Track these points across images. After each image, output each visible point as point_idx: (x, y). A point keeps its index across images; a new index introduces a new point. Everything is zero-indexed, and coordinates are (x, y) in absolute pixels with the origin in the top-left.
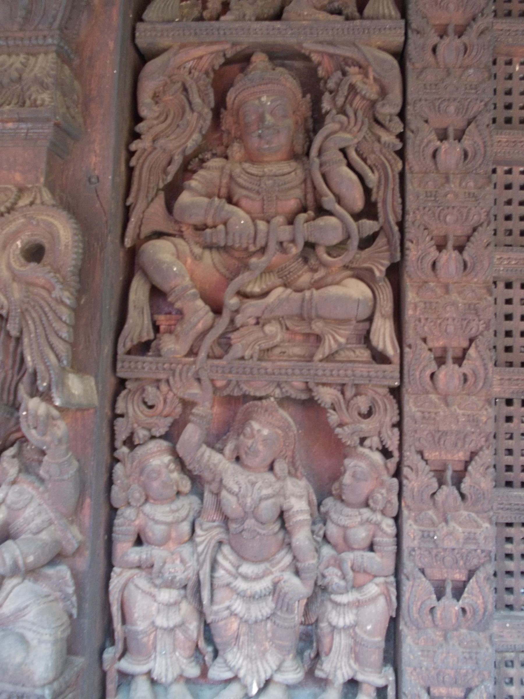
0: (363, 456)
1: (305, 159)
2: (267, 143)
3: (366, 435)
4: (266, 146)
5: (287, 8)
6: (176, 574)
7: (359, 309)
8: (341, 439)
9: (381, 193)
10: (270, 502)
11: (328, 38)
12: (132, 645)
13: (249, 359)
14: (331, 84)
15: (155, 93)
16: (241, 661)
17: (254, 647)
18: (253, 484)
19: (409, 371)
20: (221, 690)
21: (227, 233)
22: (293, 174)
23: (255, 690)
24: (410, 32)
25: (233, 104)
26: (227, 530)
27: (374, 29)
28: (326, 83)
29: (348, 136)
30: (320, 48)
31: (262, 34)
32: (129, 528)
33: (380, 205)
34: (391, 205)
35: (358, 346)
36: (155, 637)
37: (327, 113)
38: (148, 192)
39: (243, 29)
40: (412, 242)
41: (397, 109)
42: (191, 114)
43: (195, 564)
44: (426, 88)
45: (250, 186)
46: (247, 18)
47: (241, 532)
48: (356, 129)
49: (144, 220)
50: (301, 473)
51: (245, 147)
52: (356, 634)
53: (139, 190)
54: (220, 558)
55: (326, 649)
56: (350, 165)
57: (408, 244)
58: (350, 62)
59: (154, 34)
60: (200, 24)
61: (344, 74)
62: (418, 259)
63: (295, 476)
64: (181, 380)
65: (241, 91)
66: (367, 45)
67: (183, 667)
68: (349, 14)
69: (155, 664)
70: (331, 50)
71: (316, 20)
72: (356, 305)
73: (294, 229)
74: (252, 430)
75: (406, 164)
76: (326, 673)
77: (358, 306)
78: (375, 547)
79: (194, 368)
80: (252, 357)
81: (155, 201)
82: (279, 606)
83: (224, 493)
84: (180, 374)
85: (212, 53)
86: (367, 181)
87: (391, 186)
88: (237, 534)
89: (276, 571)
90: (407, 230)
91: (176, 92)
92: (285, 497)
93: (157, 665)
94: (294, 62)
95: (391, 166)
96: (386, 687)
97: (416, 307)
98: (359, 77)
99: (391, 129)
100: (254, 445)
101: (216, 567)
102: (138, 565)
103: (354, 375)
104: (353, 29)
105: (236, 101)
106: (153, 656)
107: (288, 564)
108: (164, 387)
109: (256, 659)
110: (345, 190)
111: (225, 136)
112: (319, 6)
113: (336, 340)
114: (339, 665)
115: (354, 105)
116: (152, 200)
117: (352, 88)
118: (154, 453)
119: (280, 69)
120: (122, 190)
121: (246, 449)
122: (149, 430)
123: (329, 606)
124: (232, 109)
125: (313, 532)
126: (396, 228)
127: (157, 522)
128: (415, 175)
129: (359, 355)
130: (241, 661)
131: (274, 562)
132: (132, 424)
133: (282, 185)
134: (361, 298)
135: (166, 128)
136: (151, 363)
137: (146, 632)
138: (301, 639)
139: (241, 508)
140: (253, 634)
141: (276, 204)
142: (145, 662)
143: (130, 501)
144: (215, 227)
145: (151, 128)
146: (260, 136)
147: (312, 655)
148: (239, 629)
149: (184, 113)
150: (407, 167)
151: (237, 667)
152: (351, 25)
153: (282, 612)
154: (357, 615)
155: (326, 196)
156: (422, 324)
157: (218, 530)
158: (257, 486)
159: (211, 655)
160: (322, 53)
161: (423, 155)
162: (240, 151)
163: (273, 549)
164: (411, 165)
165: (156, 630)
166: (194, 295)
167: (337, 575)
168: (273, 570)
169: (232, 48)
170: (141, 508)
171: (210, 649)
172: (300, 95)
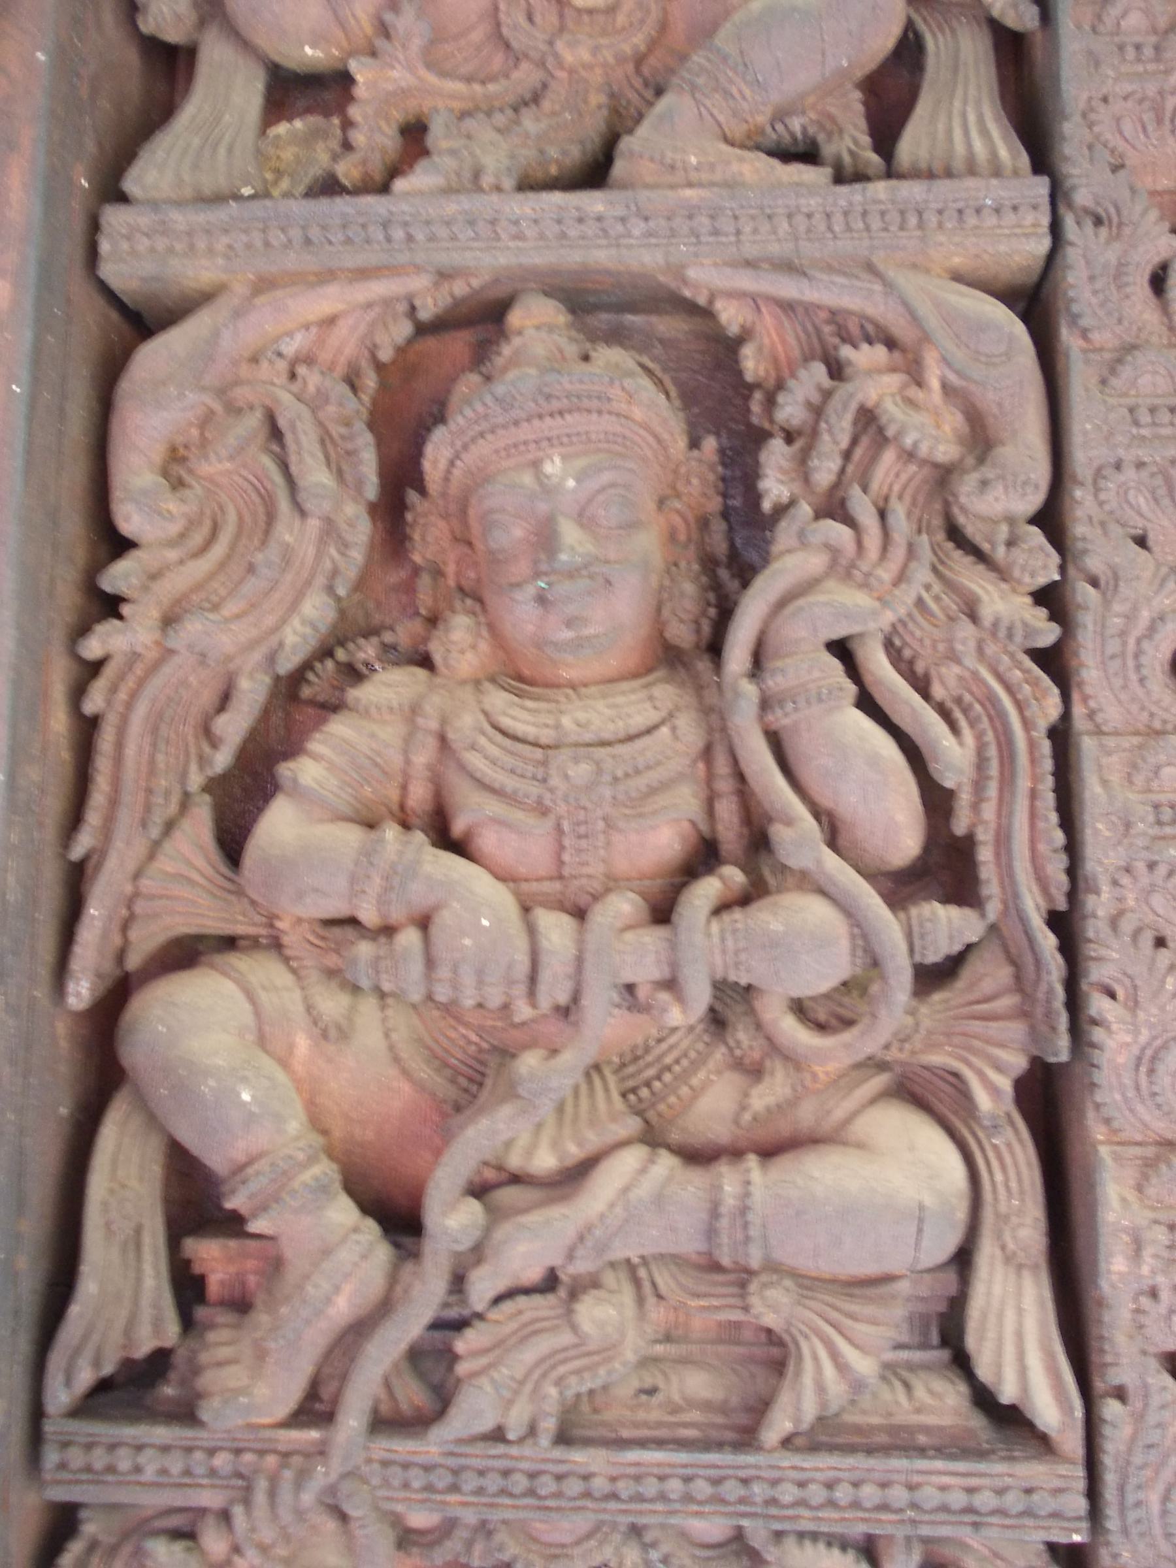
1: (703, 665)
2: (569, 624)
4: (567, 634)
5: (626, 144)
7: (925, 1243)
9: (989, 811)
11: (774, 249)
13: (521, 1441)
14: (791, 410)
15: (173, 449)
19: (1121, 1489)
21: (430, 963)
22: (665, 730)
24: (1069, 221)
25: (447, 479)
27: (940, 212)
28: (770, 402)
29: (861, 600)
30: (746, 281)
31: (542, 236)
33: (985, 854)
34: (1027, 853)
35: (918, 1356)
37: (781, 510)
38: (148, 808)
39: (472, 223)
40: (1112, 995)
41: (1034, 500)
42: (297, 523)
44: (1136, 423)
45: (510, 783)
46: (487, 180)
48: (886, 574)
49: (140, 907)
51: (492, 627)
53: (114, 802)
56: (868, 704)
57: (1098, 1005)
58: (854, 328)
59: (161, 243)
60: (324, 205)
61: (837, 370)
62: (1139, 1060)
64: (274, 1516)
65: (473, 440)
66: (914, 266)
68: (847, 159)
70: (788, 288)
71: (731, 185)
72: (914, 1229)
73: (673, 945)
75: (1076, 696)
77: (920, 1231)
79: (322, 1475)
80: (532, 1431)
81: (177, 834)
84: (272, 1494)
85: (369, 305)
86: (935, 768)
87: (1023, 783)
90: (1091, 950)
91: (240, 450)
94: (654, 319)
95: (1020, 706)
97: (1138, 1246)
98: (893, 381)
99: (1016, 573)
104: (865, 214)
105: (456, 472)
110: (853, 799)
111: (425, 582)
112: (737, 130)
113: (842, 1367)
115: (875, 486)
116: (169, 826)
117: (867, 418)
119: (609, 355)
120: (54, 805)
124: (444, 495)
126: (1048, 941)
128: (1111, 742)
129: (928, 1400)
134: (928, 1200)
135: (211, 576)
136: (165, 1449)
141: (608, 844)
144: (388, 931)
145: (154, 576)
146: (542, 599)
149: (271, 517)
150: (1078, 710)
152: (858, 198)
155: (789, 822)
156: (1162, 1308)
160: (755, 300)
161: (1138, 667)
162: (474, 647)
164: (1092, 704)
166: (322, 1189)
169: (436, 285)
172: (682, 443)
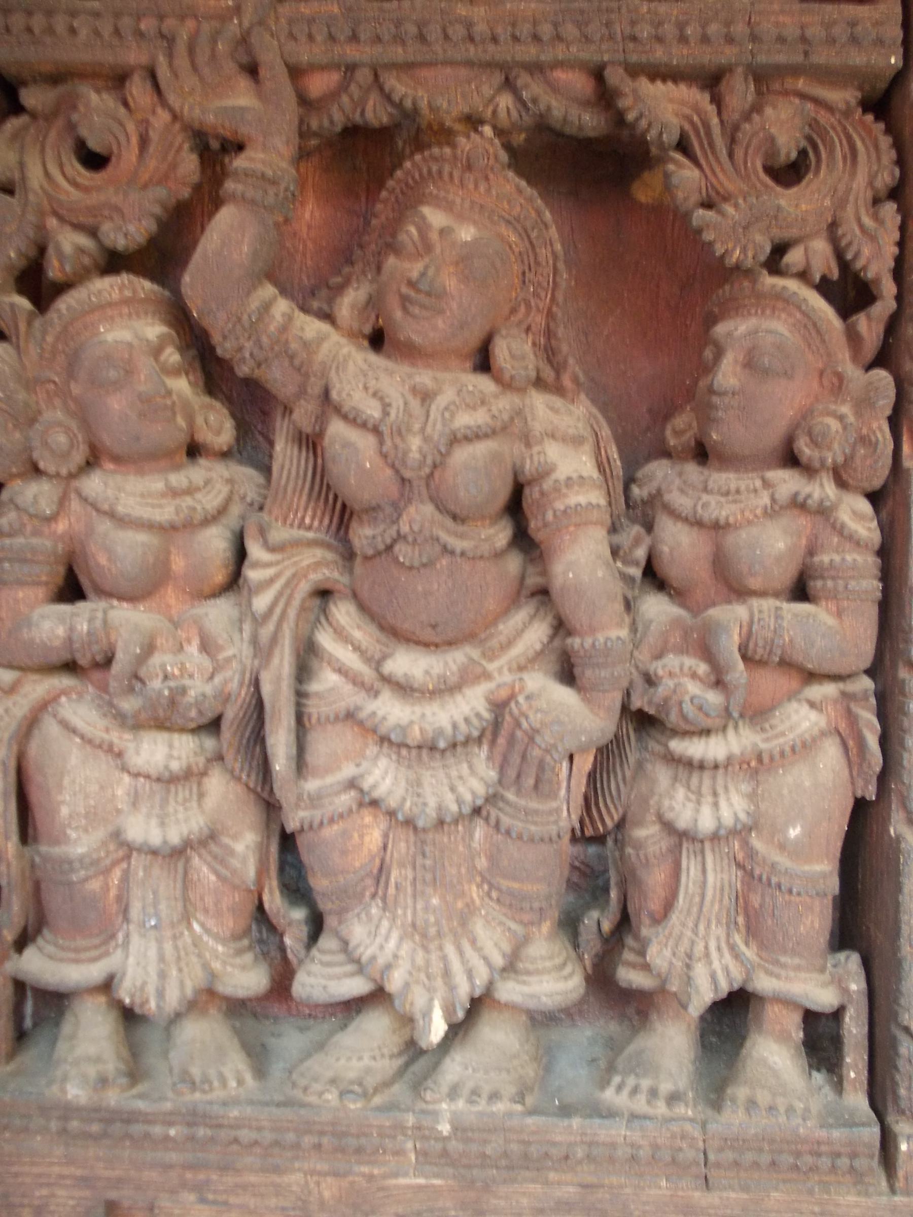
0: (782, 299)
3: (794, 232)
6: (187, 682)
8: (711, 244)
10: (481, 449)
12: (55, 901)
16: (392, 944)
17: (435, 901)
18: (426, 397)
20: (332, 1033)
23: (438, 1029)
26: (349, 555)
32: (35, 541)
36: (126, 877)
43: (247, 651)
47: (389, 548)
50: (575, 380)
52: (751, 853)
54: (325, 640)
55: (655, 904)
63: (558, 390)
64: (195, 68)
67: (216, 965)
69: (127, 957)
74: (424, 228)
76: (659, 975)
78: (816, 585)
82: (512, 773)
83: (337, 428)
84: (191, 51)
88: (378, 554)
89: (500, 670)
92: (527, 440)
93: (131, 960)
96: (837, 1015)
100: (431, 272)
101: (314, 663)
102: (66, 656)
103: (754, 38)
106: (120, 936)
107: (538, 647)
108: (138, 90)
109: (439, 934)
114: (699, 948)
118: (110, 304)
121: (405, 290)
122: (93, 232)
123: (662, 775)
125: (615, 552)
127: (123, 522)
130: (392, 944)
131: (494, 643)
132: (42, 214)
133: (376, 1090)
137: (98, 860)
138: (571, 885)
139: (389, 472)
140: (428, 862)
142: (94, 953)
143: (36, 455)
147: (606, 926)
148: (385, 848)
151: (381, 961)
153: (518, 793)
154: (752, 796)
157: (319, 553)
158: (442, 401)
159: (304, 931)
163: (491, 604)
165: (128, 857)
167: (694, 676)
168: (491, 667)
170: (76, 483)
171: (299, 914)
